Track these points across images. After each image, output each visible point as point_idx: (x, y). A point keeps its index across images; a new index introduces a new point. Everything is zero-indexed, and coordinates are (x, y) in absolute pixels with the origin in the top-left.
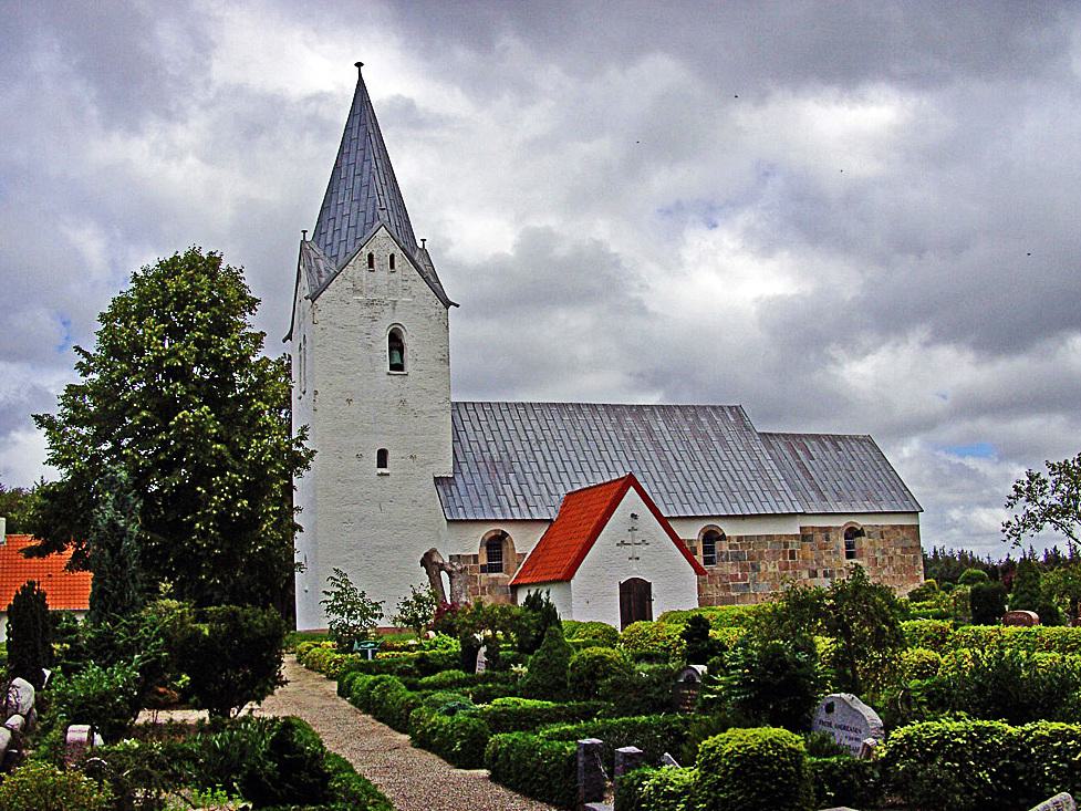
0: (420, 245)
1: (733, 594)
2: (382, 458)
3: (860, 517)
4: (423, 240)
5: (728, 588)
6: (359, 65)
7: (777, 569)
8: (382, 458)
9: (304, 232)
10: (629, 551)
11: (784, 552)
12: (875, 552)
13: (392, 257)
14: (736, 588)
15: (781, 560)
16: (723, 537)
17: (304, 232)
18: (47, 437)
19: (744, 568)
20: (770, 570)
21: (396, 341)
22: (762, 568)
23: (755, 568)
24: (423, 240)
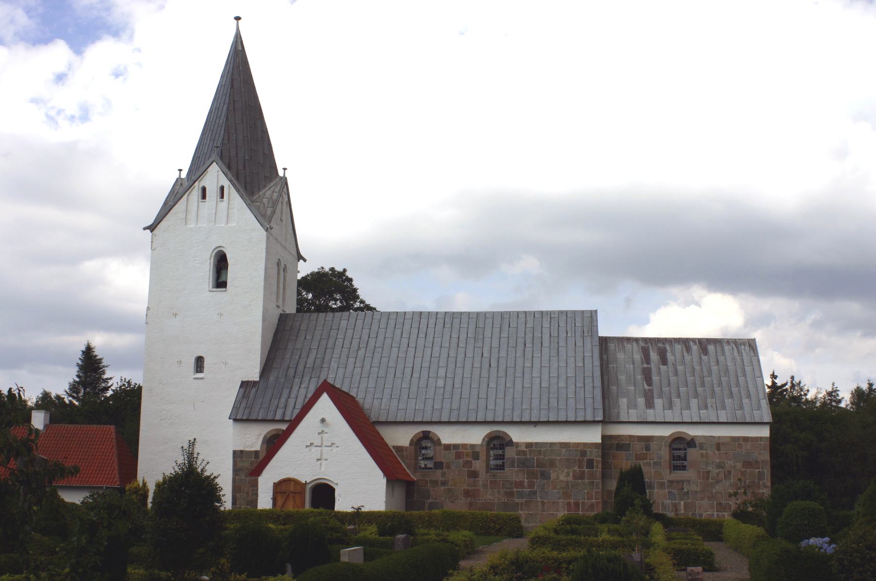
0: (281, 173)
1: (516, 500)
2: (199, 364)
3: (691, 426)
4: (285, 169)
5: (510, 494)
6: (238, 18)
7: (570, 478)
8: (199, 364)
9: (180, 170)
10: (315, 452)
11: (580, 461)
12: (707, 464)
13: (222, 188)
14: (521, 494)
15: (576, 468)
16: (510, 443)
17: (180, 170)
18: (806, 388)
19: (531, 475)
20: (562, 478)
21: (221, 262)
22: (553, 476)
23: (545, 476)
24: (285, 169)
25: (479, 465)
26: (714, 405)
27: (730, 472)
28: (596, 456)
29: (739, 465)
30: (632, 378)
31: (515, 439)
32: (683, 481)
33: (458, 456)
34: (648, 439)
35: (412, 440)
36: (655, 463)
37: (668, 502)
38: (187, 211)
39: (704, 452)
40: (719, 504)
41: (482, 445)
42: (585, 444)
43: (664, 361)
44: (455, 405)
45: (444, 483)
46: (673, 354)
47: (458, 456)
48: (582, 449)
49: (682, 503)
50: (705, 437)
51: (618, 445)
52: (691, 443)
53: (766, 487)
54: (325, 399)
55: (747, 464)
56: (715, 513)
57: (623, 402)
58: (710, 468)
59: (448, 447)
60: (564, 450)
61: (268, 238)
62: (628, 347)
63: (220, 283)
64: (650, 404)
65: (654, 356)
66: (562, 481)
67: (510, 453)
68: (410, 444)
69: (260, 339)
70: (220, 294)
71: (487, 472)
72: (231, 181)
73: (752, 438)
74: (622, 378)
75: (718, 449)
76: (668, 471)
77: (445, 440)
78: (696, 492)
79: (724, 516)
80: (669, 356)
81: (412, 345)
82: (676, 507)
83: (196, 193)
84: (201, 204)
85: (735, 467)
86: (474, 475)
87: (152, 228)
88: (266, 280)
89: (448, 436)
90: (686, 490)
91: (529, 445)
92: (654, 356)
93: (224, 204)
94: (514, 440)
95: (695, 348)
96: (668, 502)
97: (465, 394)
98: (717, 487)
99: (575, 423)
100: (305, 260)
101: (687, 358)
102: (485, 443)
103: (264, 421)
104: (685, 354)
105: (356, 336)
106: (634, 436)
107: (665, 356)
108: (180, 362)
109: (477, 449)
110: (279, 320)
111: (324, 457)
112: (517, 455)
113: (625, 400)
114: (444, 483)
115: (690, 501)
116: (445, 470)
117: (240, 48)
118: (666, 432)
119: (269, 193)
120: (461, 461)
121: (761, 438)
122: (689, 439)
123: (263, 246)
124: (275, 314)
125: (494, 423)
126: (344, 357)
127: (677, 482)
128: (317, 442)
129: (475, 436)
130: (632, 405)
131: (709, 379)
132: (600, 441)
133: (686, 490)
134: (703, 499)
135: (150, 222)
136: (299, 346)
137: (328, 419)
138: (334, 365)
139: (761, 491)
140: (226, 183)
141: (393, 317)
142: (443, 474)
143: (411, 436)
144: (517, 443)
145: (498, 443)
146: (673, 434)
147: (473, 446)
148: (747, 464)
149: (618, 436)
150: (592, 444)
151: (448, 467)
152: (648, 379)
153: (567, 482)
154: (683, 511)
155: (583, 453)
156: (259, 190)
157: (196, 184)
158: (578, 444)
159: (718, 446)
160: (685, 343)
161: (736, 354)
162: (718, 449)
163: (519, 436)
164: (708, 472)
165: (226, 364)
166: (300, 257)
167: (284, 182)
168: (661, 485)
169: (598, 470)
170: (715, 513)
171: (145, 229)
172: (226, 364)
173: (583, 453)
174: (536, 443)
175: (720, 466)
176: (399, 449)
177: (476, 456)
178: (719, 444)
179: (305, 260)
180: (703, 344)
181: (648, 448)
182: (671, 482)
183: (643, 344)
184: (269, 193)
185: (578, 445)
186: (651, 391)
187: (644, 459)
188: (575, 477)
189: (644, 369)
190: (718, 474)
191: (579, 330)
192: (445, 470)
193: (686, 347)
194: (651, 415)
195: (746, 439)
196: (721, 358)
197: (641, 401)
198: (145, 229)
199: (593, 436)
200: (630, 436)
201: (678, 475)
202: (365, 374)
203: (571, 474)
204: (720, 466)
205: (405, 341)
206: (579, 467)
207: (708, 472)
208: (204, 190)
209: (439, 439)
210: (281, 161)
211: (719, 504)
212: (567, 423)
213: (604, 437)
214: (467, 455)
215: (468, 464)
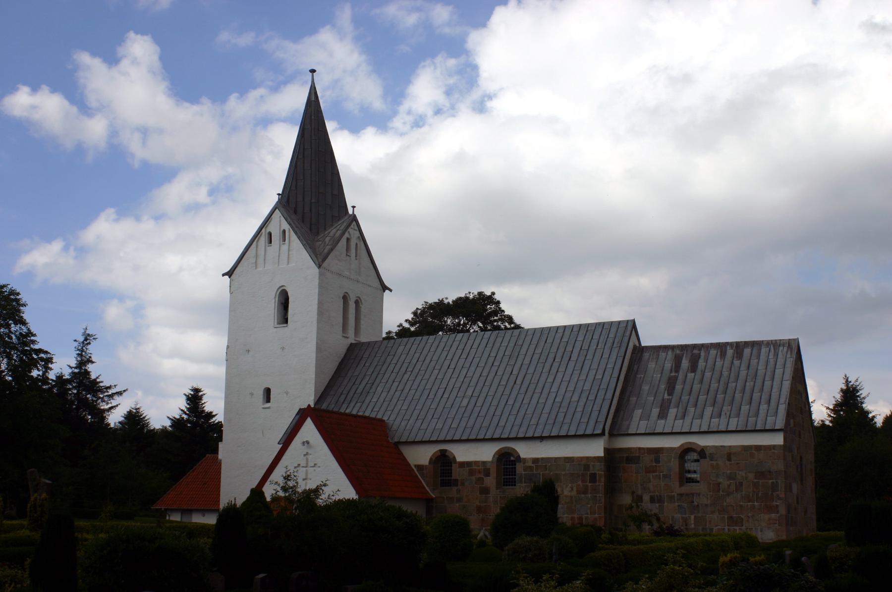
0: (350, 212)
7: (574, 493)
13: (284, 231)
15: (580, 483)
24: (354, 207)
25: (490, 482)
26: (728, 413)
27: (741, 484)
28: (599, 470)
29: (751, 476)
30: (656, 387)
31: (523, 455)
32: (693, 494)
33: (472, 473)
34: (657, 451)
35: (431, 459)
36: (665, 476)
37: (678, 516)
38: (257, 256)
39: (714, 463)
40: (730, 518)
41: (492, 462)
42: (588, 458)
43: (693, 368)
44: (424, 426)
45: (459, 500)
46: (706, 361)
47: (472, 473)
48: (586, 463)
49: (692, 517)
50: (716, 447)
51: (628, 458)
52: (702, 453)
53: (780, 499)
54: (309, 424)
55: (760, 474)
56: (727, 527)
57: (638, 412)
58: (720, 480)
59: (462, 464)
60: (568, 465)
61: (321, 274)
62: (662, 355)
63: (284, 319)
64: (663, 415)
65: (685, 364)
66: (566, 496)
67: (519, 469)
68: (430, 462)
69: (314, 369)
70: (284, 331)
71: (497, 489)
72: (290, 225)
73: (765, 446)
74: (646, 388)
75: (729, 459)
76: (677, 484)
77: (459, 459)
78: (706, 505)
79: (735, 530)
80: (701, 364)
81: (452, 366)
82: (686, 521)
83: (263, 239)
84: (268, 248)
85: (746, 478)
86: (485, 491)
87: (230, 274)
88: (320, 313)
89: (463, 453)
90: (696, 503)
91: (536, 460)
92: (685, 364)
93: (285, 247)
94: (522, 456)
95: (730, 352)
96: (678, 516)
97: (483, 413)
98: (728, 500)
99: (575, 436)
100: (391, 290)
101: (719, 363)
102: (495, 460)
103: (492, 440)
104: (718, 360)
105: (407, 361)
106: (643, 449)
107: (697, 362)
108: (252, 394)
109: (488, 466)
110: (348, 350)
111: (309, 476)
112: (525, 470)
113: (640, 411)
114: (459, 500)
115: (700, 515)
116: (460, 487)
117: (313, 99)
118: (675, 443)
119: (334, 231)
120: (474, 478)
121: (774, 447)
122: (699, 450)
123: (316, 282)
124: (339, 344)
125: (500, 439)
126: (390, 381)
127: (687, 495)
128: (303, 463)
129: (486, 453)
130: (646, 416)
131: (734, 384)
132: (601, 454)
133: (696, 503)
134: (713, 512)
135: (227, 269)
136: (356, 373)
137: (311, 442)
138: (380, 389)
139: (775, 503)
140: (286, 226)
141: (622, 325)
142: (458, 491)
143: (430, 454)
144: (525, 459)
145: (507, 460)
146: (683, 445)
147: (484, 463)
148: (760, 474)
149: (629, 449)
150: (595, 457)
151: (463, 484)
152: (671, 389)
153: (572, 497)
154: (693, 526)
155: (586, 468)
156: (325, 230)
157: (263, 230)
158: (582, 458)
159: (729, 456)
160: (721, 347)
161: (771, 356)
162: (729, 459)
163: (527, 451)
164: (719, 484)
165: (287, 393)
166: (385, 288)
167: (354, 218)
168: (671, 499)
169: (601, 484)
170: (727, 527)
171: (223, 275)
172: (287, 393)
173: (586, 468)
174: (542, 459)
175: (731, 477)
176: (420, 467)
177: (487, 473)
178: (729, 454)
179: (391, 290)
180: (739, 348)
181: (657, 461)
182: (681, 495)
183: (678, 352)
184: (334, 231)
185: (581, 459)
186: (670, 401)
187: (654, 471)
188: (579, 492)
189: (670, 378)
190: (729, 486)
191: (610, 341)
192: (460, 487)
193: (721, 352)
194: (660, 426)
195: (758, 448)
196: (754, 362)
197: (656, 411)
198: (223, 275)
199: (595, 449)
200: (640, 449)
201: (688, 488)
202: (402, 398)
203: (575, 489)
204: (731, 477)
205: (447, 363)
206: (583, 481)
207: (719, 484)
208: (270, 234)
209: (454, 457)
210: (351, 198)
211: (730, 518)
212: (567, 437)
213: (606, 450)
214: (479, 472)
215: (480, 480)
